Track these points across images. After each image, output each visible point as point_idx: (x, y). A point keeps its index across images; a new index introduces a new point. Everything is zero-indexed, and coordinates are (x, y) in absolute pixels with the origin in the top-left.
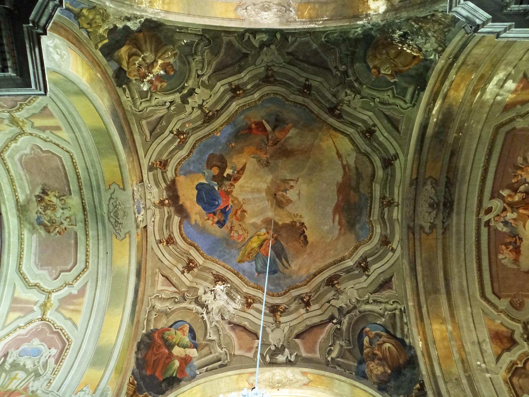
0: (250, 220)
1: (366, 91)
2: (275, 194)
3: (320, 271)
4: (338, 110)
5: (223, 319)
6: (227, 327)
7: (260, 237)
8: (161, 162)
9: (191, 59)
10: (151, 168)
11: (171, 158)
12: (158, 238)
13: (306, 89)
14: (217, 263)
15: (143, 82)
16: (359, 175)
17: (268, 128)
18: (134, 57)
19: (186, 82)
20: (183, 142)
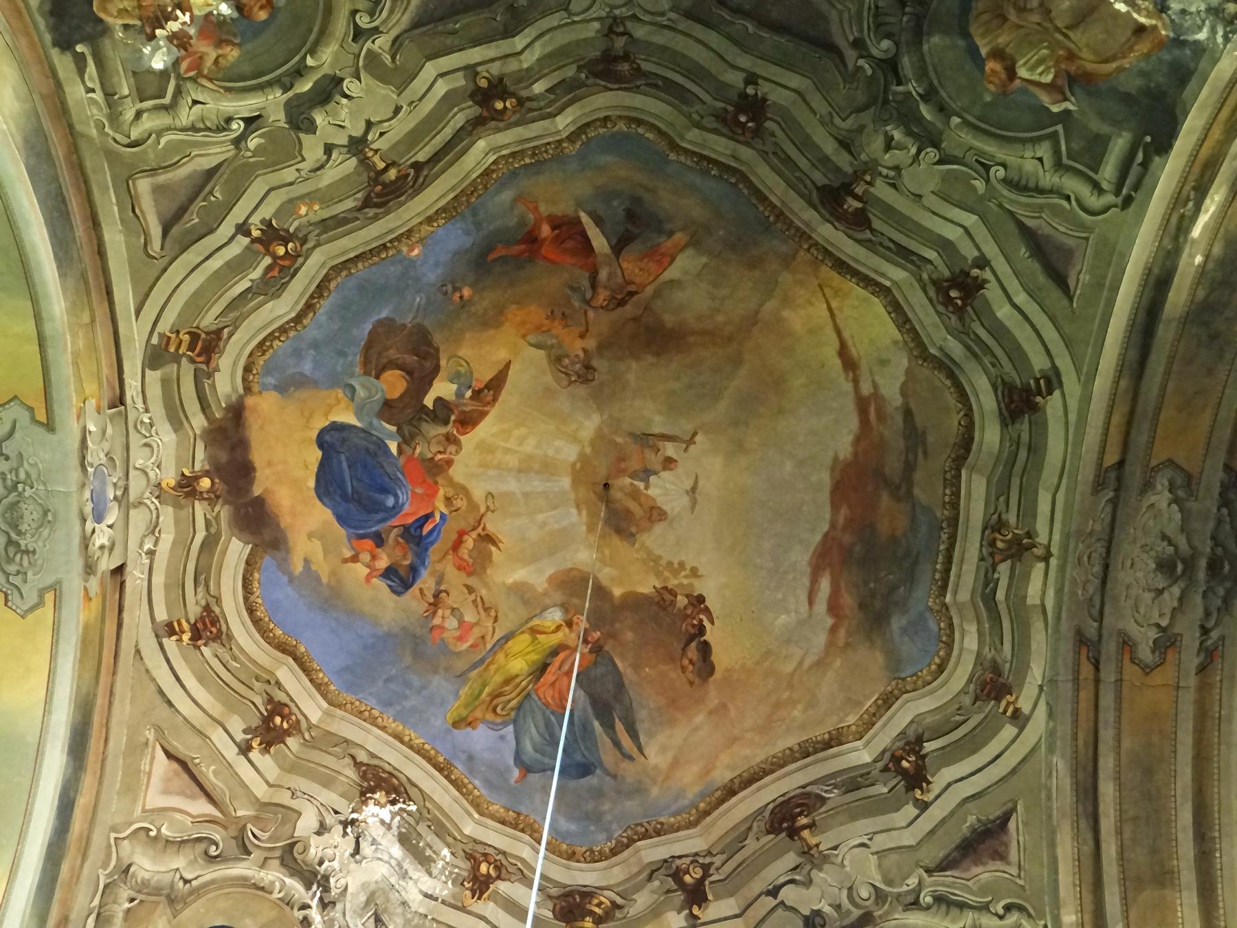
0: (508, 572)
1: (960, 137)
2: (606, 486)
3: (750, 779)
4: (856, 197)
7: (541, 637)
8: (194, 337)
10: (156, 357)
11: (235, 325)
12: (162, 615)
13: (746, 114)
14: (373, 721)
15: (152, 37)
16: (914, 436)
17: (599, 242)
19: (312, 52)
20: (282, 269)
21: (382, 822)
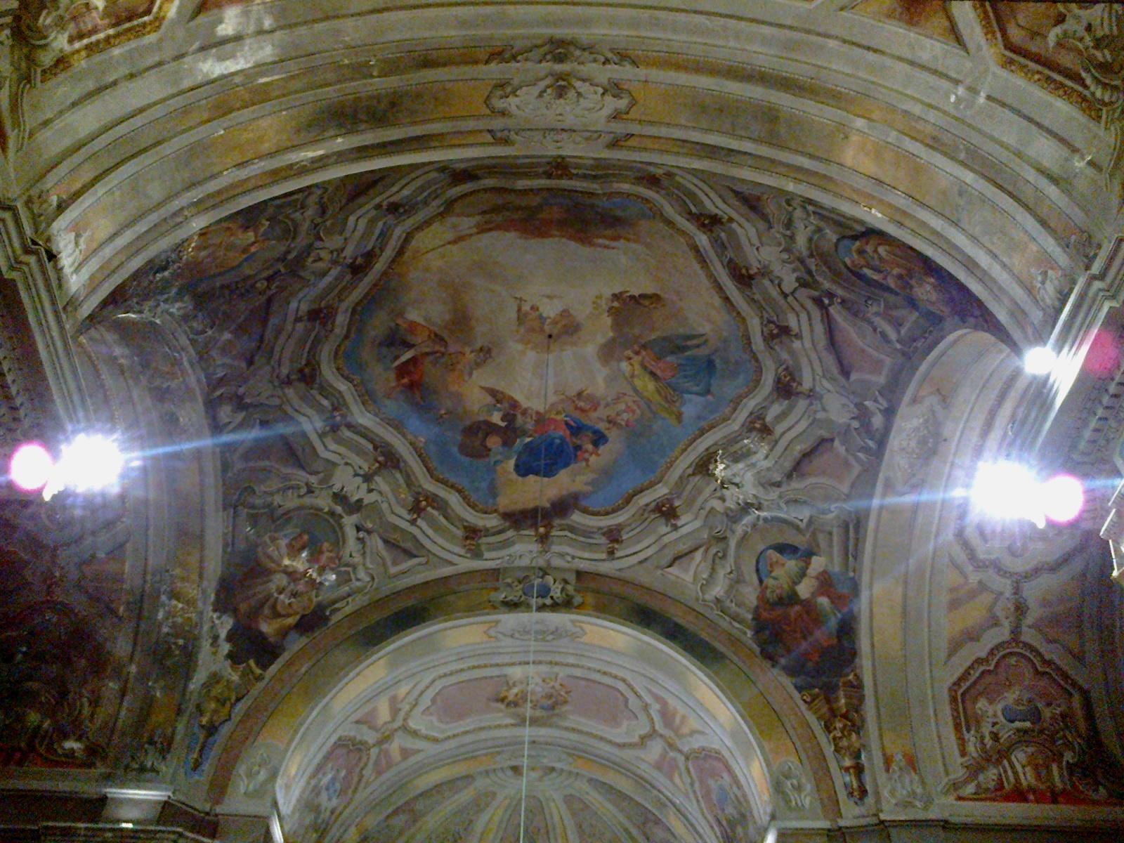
2: (550, 336)
3: (719, 288)
5: (778, 485)
6: (795, 484)
7: (636, 373)
8: (467, 538)
9: (280, 511)
10: (477, 555)
11: (462, 520)
12: (604, 556)
13: (320, 316)
14: (672, 463)
15: (321, 583)
16: (495, 210)
18: (279, 608)
19: (321, 510)
20: (433, 500)
21: (725, 469)
